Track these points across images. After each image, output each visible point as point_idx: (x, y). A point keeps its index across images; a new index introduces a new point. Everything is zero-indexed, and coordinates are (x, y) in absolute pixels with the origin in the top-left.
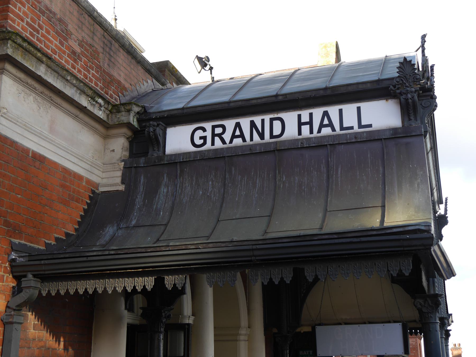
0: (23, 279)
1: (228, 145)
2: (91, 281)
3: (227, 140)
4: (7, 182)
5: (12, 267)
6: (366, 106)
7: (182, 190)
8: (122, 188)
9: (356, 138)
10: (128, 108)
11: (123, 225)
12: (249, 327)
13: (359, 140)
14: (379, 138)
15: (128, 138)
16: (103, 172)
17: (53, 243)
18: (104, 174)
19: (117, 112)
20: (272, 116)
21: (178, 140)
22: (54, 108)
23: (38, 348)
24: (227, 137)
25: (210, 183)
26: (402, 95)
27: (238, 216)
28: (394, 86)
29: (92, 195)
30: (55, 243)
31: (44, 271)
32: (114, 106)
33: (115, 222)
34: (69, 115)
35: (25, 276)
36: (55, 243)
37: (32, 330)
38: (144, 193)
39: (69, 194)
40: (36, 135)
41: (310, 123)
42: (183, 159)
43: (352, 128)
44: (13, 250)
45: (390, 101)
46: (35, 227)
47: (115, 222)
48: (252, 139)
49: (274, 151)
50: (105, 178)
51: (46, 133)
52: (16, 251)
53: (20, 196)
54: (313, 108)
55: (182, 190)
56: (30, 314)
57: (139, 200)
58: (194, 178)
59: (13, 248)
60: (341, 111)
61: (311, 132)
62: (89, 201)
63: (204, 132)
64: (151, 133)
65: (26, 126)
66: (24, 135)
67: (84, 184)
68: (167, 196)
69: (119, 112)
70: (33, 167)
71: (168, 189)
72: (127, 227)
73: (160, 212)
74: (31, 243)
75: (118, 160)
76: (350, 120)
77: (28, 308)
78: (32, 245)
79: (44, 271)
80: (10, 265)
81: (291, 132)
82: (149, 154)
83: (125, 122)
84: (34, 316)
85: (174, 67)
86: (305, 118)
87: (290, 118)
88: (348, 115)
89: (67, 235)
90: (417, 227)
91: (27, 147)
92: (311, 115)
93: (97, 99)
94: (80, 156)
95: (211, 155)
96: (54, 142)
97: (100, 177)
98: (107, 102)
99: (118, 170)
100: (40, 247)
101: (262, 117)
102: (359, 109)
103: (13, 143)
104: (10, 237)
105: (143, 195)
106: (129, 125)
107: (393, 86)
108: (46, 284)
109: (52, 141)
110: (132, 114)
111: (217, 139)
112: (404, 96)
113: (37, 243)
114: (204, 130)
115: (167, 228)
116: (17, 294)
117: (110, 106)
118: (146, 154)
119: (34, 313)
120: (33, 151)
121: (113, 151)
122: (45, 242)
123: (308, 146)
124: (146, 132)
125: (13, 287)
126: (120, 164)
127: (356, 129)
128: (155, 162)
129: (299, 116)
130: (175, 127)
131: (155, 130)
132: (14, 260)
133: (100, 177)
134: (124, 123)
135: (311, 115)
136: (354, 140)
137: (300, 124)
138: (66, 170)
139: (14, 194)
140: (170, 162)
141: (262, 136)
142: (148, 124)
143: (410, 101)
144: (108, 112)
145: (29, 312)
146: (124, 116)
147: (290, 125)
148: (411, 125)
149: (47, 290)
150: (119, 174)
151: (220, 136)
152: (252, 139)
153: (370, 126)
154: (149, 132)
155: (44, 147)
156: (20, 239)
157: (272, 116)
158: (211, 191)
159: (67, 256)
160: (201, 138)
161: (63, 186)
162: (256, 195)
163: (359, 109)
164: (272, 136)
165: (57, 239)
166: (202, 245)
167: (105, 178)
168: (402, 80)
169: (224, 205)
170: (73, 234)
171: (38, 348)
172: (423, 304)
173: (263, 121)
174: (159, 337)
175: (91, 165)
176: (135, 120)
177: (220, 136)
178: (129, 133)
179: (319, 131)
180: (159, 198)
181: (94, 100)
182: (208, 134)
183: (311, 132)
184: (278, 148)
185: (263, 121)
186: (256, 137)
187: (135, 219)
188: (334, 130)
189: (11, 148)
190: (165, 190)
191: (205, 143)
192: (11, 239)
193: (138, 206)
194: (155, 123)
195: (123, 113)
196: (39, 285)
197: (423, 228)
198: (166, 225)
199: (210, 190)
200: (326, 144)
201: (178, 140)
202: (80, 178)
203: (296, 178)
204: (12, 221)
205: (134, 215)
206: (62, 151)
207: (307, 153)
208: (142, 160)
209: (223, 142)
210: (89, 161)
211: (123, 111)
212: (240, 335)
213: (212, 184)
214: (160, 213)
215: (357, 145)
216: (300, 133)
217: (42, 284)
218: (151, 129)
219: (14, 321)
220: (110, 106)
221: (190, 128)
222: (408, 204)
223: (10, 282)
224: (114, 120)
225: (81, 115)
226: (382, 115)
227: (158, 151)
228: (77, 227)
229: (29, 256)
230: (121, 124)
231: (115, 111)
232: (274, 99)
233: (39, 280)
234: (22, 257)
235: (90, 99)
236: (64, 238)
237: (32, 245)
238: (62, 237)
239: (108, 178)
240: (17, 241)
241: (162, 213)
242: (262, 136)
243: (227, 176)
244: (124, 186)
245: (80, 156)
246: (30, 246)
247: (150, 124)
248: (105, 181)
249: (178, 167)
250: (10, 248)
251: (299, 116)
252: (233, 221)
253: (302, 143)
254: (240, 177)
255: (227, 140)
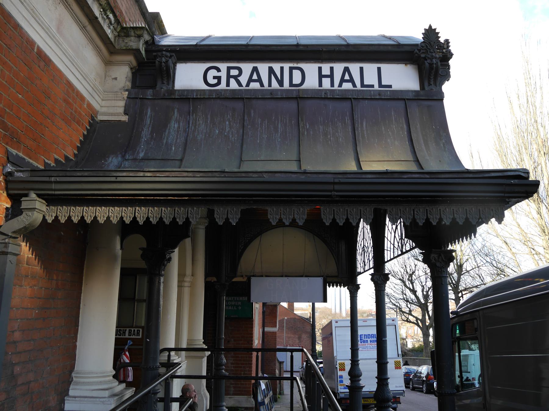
0: (23, 199)
1: (244, 87)
2: (116, 208)
3: (244, 83)
4: (7, 73)
5: (7, 182)
6: (386, 68)
7: (195, 127)
8: (125, 118)
9: (379, 95)
10: (139, 33)
11: (129, 156)
12: (192, 275)
13: (383, 97)
14: (402, 98)
15: (131, 69)
16: (103, 100)
17: (53, 164)
18: (104, 102)
19: (125, 36)
20: (292, 65)
21: (189, 76)
22: (63, 7)
23: (31, 287)
24: (244, 79)
25: (227, 123)
26: (426, 60)
27: (262, 158)
28: (419, 50)
29: (91, 122)
30: (54, 165)
31: (55, 190)
32: (123, 28)
33: (119, 153)
34: (76, 22)
35: (26, 195)
36: (54, 165)
37: (25, 265)
38: (151, 126)
39: (71, 113)
40: (43, 28)
41: (331, 76)
42: (196, 95)
43: (372, 86)
44: (9, 161)
45: (409, 66)
46: (35, 140)
47: (119, 153)
48: (270, 85)
49: (296, 98)
50: (105, 107)
51: (54, 30)
52: (13, 164)
53: (20, 96)
54: (335, 63)
55: (195, 127)
56: (23, 244)
57: (146, 133)
58: (209, 116)
59: (9, 159)
60: (361, 69)
61: (332, 84)
62: (88, 128)
63: (218, 72)
64: (163, 64)
65: (33, 12)
66: (31, 22)
67: (85, 106)
68: (178, 132)
69: (128, 36)
70: (37, 66)
71: (179, 124)
72: (135, 160)
73: (172, 146)
74: (30, 158)
75: (120, 89)
76: (371, 79)
77: (22, 237)
78: (31, 161)
79: (55, 190)
80: (5, 180)
81: (312, 82)
82: (158, 86)
83: (134, 48)
84: (28, 248)
85: (162, 21)
86: (326, 70)
87: (311, 69)
88: (370, 73)
89: (67, 158)
90: (517, 173)
91: (32, 39)
92: (332, 69)
93: (108, 13)
94: (84, 74)
95: (228, 95)
96: (61, 46)
97: (99, 104)
98: (118, 22)
99: (120, 100)
100: (39, 166)
101: (282, 65)
102: (379, 69)
103: (17, 26)
104: (7, 144)
105: (150, 129)
106: (136, 52)
107: (418, 50)
108: (53, 208)
109: (60, 44)
110: (142, 42)
111: (232, 81)
112: (429, 61)
113: (36, 160)
114: (219, 70)
115: (183, 163)
116: (11, 219)
117: (119, 26)
118: (153, 86)
119: (28, 245)
120: (38, 47)
121: (116, 79)
122: (44, 161)
123: (331, 97)
124: (157, 62)
125: (7, 209)
126: (123, 93)
127: (376, 87)
128: (164, 95)
129: (320, 69)
130: (186, 63)
131: (167, 61)
132: (10, 174)
133: (99, 104)
134: (133, 50)
135: (332, 69)
136: (378, 97)
137: (321, 76)
138: (69, 84)
139: (14, 91)
140: (182, 97)
141: (281, 83)
142: (159, 54)
143: (435, 66)
144: (117, 34)
145: (23, 241)
146: (133, 42)
147: (310, 75)
148: (432, 89)
149: (54, 215)
150: (122, 103)
151: (236, 77)
152: (270, 85)
153: (390, 86)
154: (160, 62)
155: (50, 47)
156: (18, 149)
157: (292, 65)
158: (229, 131)
159: (86, 174)
160: (215, 78)
161: (65, 101)
162: (280, 140)
163: (379, 69)
164: (291, 84)
165: (56, 161)
166: (267, 174)
167: (105, 107)
168: (427, 46)
169: (245, 146)
170: (72, 160)
171: (31, 287)
172: (437, 258)
173: (282, 69)
174: (160, 280)
175: (92, 88)
176: (143, 49)
177: (236, 77)
178: (134, 63)
179: (340, 85)
180: (169, 133)
181: (106, 14)
182: (223, 75)
183: (332, 84)
184: (301, 96)
185: (282, 69)
186: (275, 84)
187: (143, 151)
188: (354, 85)
189: (14, 31)
190: (176, 126)
191: (219, 83)
192: (8, 147)
193: (144, 139)
194: (168, 54)
195: (132, 38)
196: (44, 208)
197: (522, 174)
198: (181, 160)
199: (227, 129)
200: (350, 97)
201: (189, 76)
202: (82, 98)
203: (321, 127)
204: (10, 124)
205: (140, 147)
206: (68, 60)
207: (331, 105)
208: (149, 93)
209: (240, 84)
210: (92, 82)
211: (132, 36)
212: (185, 282)
213: (230, 124)
214: (171, 149)
215: (381, 102)
216: (320, 84)
217: (48, 208)
218: (164, 60)
219: (9, 251)
220: (119, 26)
221: (205, 66)
222: (440, 161)
223: (4, 201)
224: (120, 44)
225: (89, 28)
226: (401, 78)
227: (168, 84)
228: (76, 152)
229: (31, 171)
230: (129, 49)
231: (123, 34)
232: (295, 48)
233: (44, 202)
234: (21, 171)
235: (102, 10)
236: (64, 162)
237: (31, 161)
238: (62, 160)
239: (108, 107)
240: (14, 152)
241: (173, 148)
242: (281, 83)
243: (246, 118)
244: (127, 117)
245: (84, 74)
246: (29, 162)
247: (163, 54)
248: (104, 110)
249: (191, 103)
250: (6, 158)
251: (320, 69)
252: (259, 162)
253: (325, 94)
254: (260, 120)
255: (244, 83)
